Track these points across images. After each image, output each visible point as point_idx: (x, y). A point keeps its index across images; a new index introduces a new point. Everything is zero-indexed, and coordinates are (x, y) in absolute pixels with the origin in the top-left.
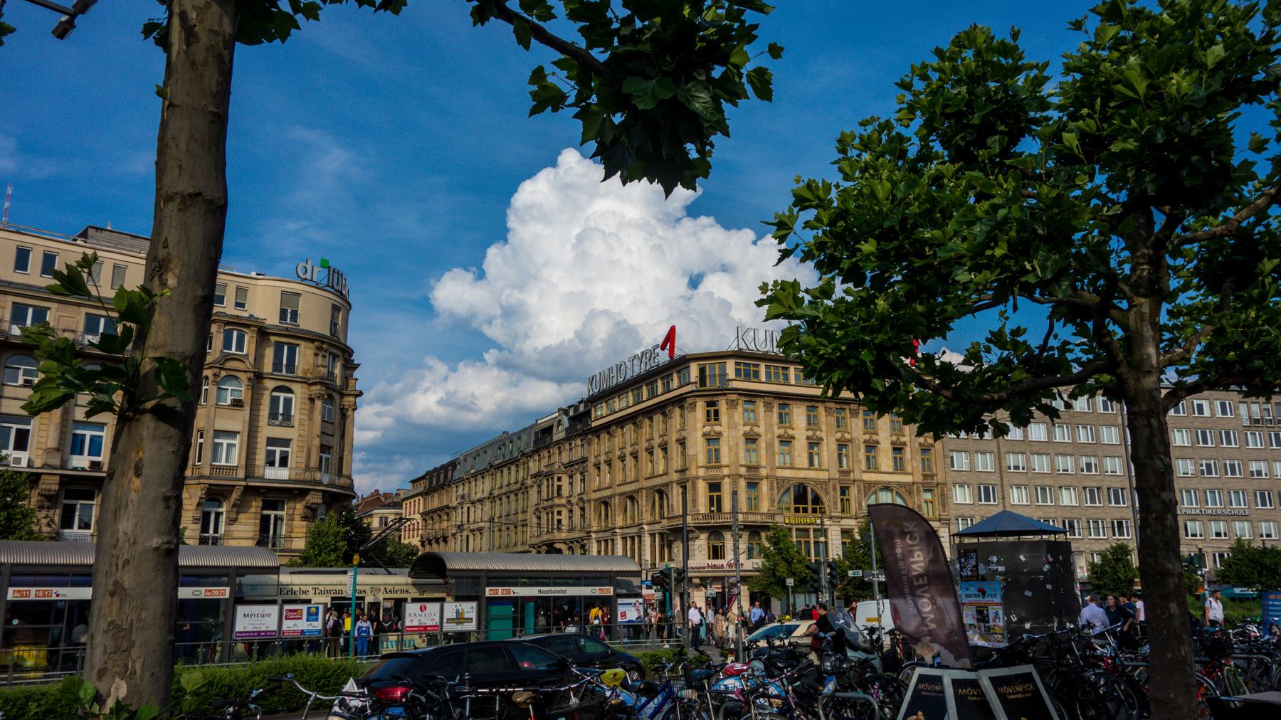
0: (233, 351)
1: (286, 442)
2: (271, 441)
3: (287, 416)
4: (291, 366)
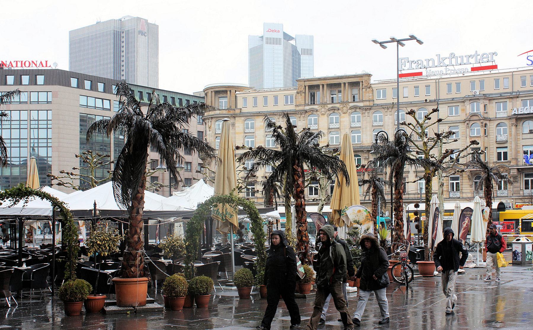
0: (475, 112)
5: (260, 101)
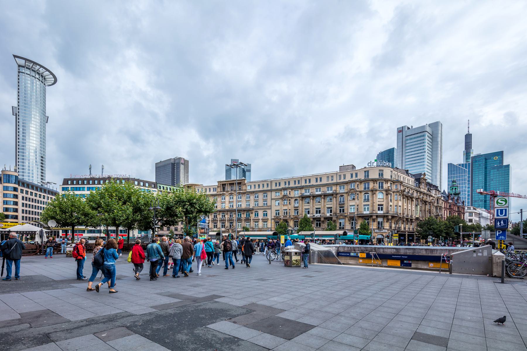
1: (368, 205)
2: (364, 205)
3: (368, 199)
4: (368, 188)
5: (354, 175)
